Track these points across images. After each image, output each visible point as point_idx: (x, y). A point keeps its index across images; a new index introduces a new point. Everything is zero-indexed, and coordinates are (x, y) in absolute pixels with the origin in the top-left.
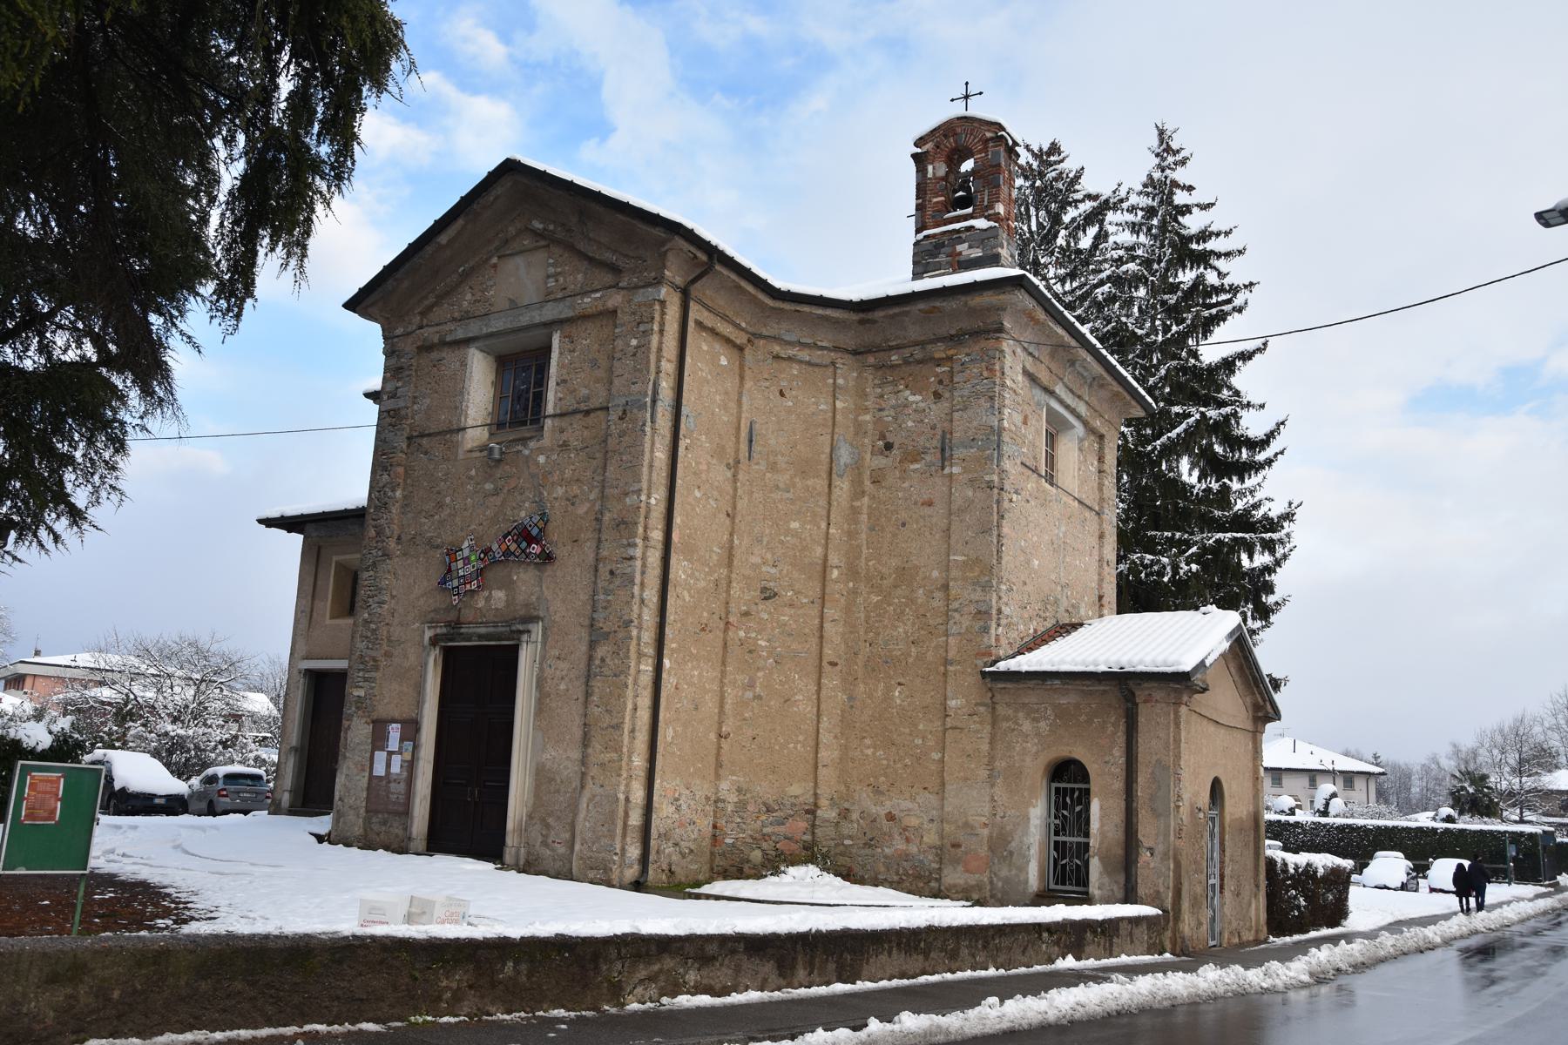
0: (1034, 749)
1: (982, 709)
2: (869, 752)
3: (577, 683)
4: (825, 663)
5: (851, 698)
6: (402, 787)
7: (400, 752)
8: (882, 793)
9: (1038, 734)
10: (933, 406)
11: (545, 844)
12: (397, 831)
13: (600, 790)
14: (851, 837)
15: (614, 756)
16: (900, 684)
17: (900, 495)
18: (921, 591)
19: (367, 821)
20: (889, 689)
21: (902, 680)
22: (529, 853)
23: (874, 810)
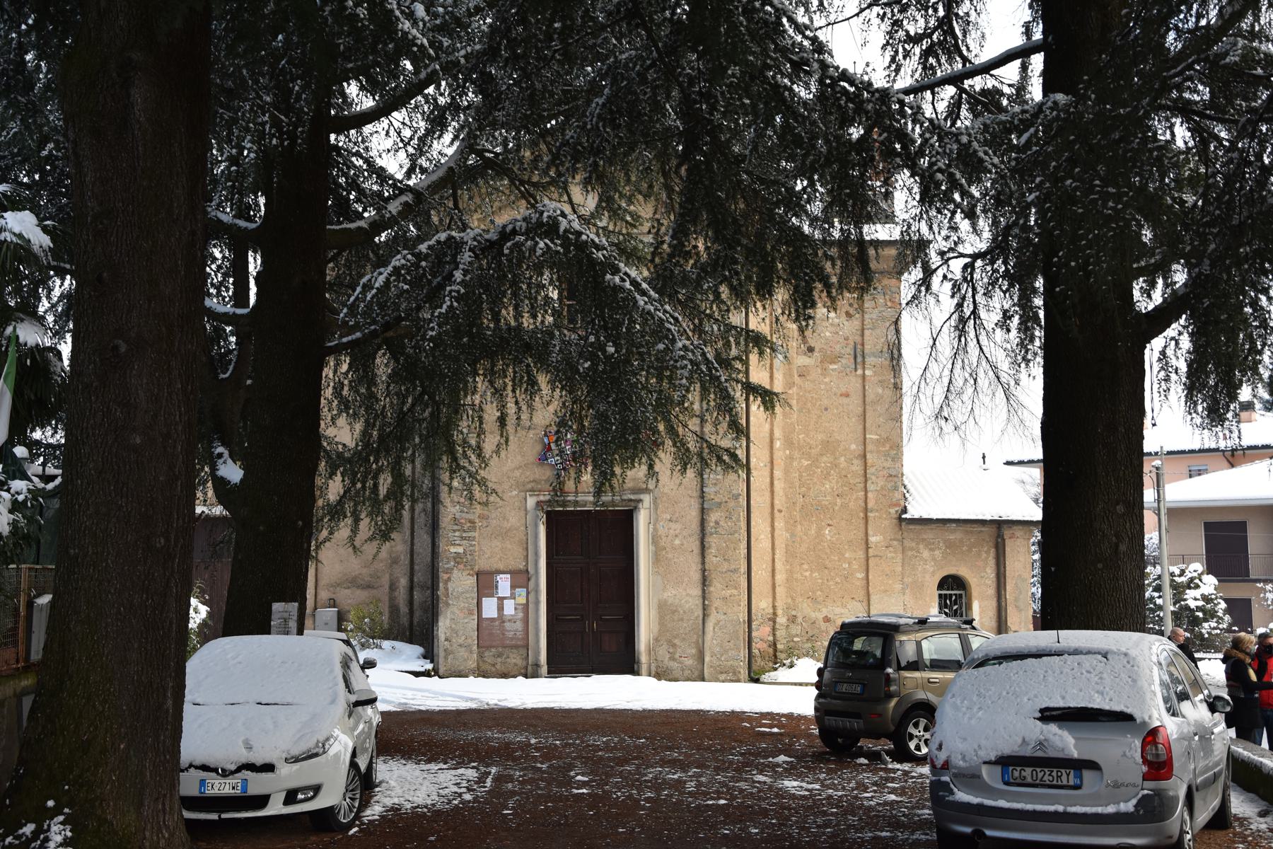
0: (932, 569)
1: (895, 543)
2: (807, 574)
3: (691, 540)
4: (776, 511)
5: (793, 535)
6: (519, 626)
7: (513, 597)
8: (818, 603)
9: (934, 559)
10: (846, 323)
11: (672, 659)
12: (514, 661)
13: (723, 617)
14: (797, 636)
15: (735, 592)
16: (829, 525)
17: (823, 387)
18: (843, 459)
19: (481, 656)
20: (820, 529)
21: (830, 522)
22: (658, 667)
23: (813, 615)
